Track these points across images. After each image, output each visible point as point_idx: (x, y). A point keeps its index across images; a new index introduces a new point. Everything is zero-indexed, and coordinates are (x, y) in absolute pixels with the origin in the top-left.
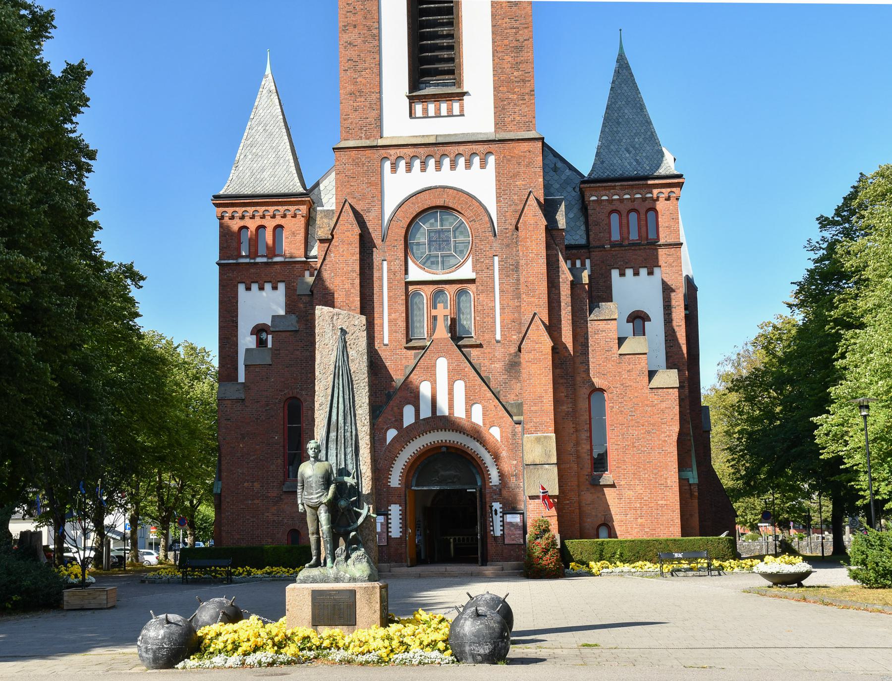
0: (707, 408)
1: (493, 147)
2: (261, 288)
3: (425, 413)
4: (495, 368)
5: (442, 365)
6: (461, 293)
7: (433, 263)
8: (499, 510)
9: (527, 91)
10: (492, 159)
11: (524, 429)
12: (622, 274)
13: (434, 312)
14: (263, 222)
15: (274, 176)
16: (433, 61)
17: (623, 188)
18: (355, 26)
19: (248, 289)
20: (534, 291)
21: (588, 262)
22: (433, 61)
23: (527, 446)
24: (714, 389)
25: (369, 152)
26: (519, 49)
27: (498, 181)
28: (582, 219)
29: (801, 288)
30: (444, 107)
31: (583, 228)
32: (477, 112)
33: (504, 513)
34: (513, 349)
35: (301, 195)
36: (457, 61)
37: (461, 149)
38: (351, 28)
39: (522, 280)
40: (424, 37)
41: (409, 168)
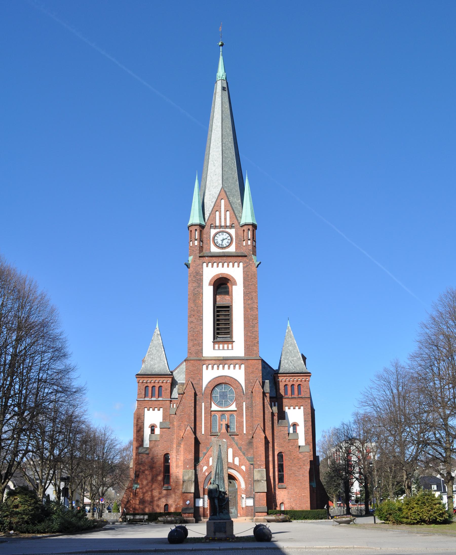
0: (318, 456)
1: (243, 362)
2: (154, 410)
7: (221, 404)
8: (244, 497)
9: (256, 342)
10: (243, 366)
11: (254, 467)
13: (221, 423)
15: (159, 367)
18: (194, 316)
21: (276, 403)
23: (255, 474)
24: (320, 440)
25: (198, 362)
27: (245, 374)
28: (274, 387)
30: (226, 346)
31: (275, 390)
32: (238, 348)
34: (250, 437)
35: (170, 375)
36: (230, 329)
37: (232, 362)
40: (218, 320)
41: (213, 368)
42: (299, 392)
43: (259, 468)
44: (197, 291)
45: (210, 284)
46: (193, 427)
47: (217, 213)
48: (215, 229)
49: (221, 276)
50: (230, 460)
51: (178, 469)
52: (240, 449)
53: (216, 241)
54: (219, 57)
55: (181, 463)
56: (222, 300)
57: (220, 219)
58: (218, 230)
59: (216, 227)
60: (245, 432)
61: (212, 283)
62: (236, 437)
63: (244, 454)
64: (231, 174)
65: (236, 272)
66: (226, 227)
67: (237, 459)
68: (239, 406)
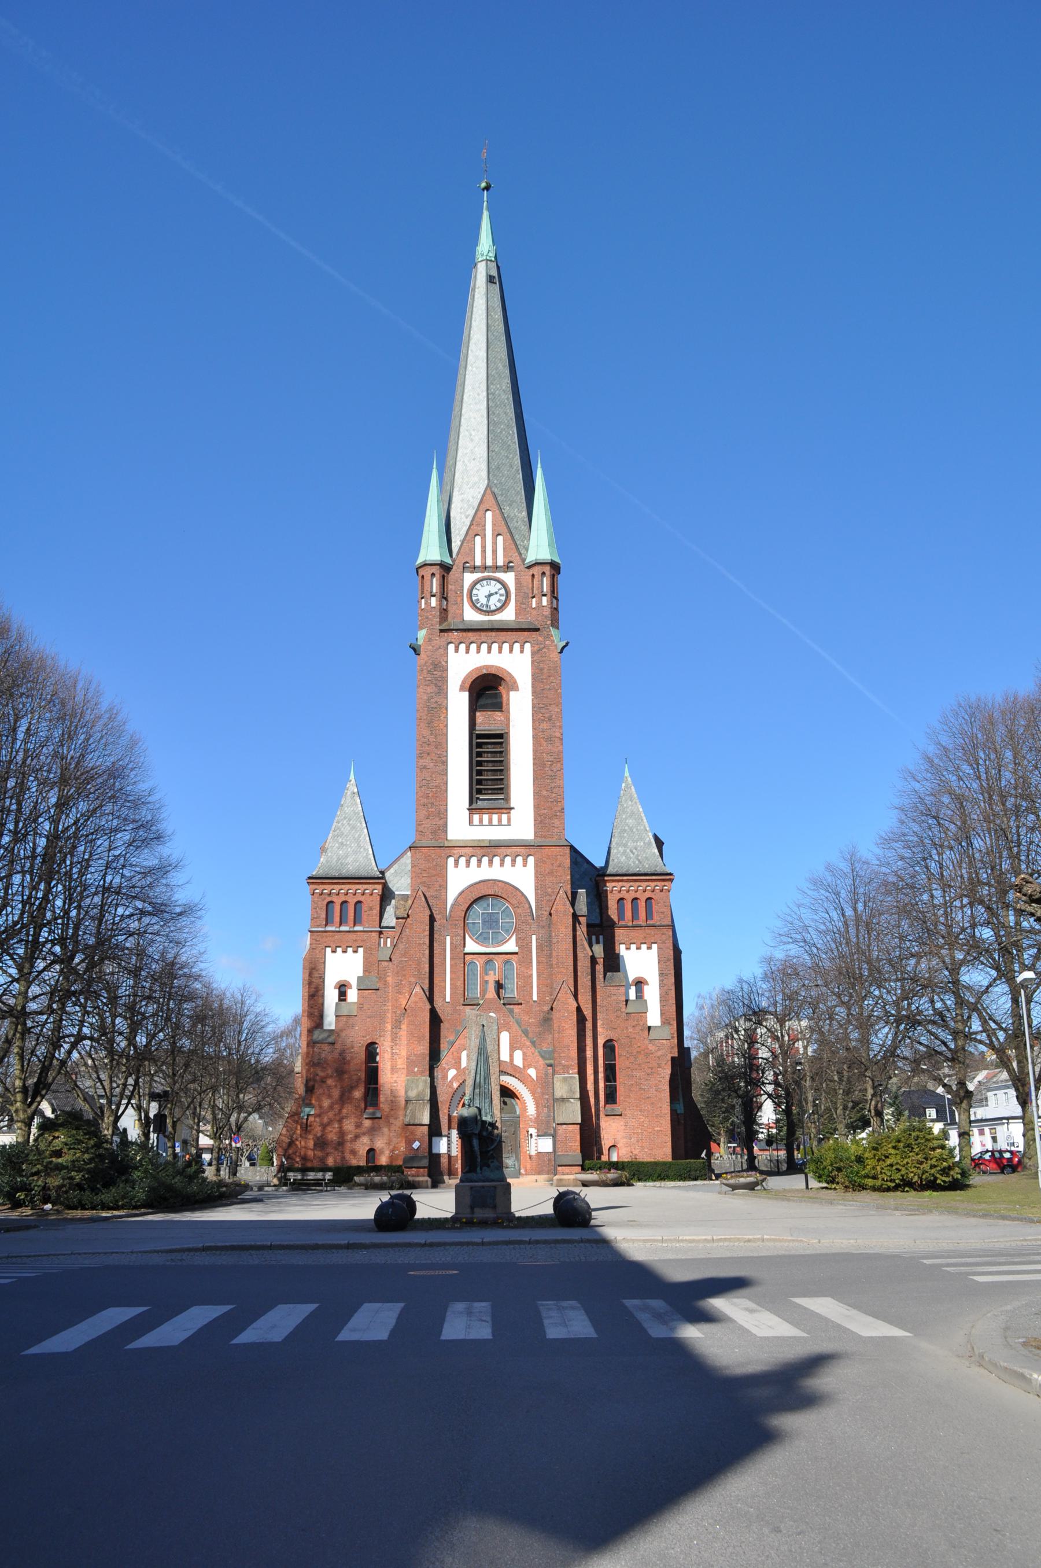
1: (532, 850)
2: (345, 952)
6: (507, 962)
7: (485, 938)
11: (554, 1071)
12: (457, 650)
13: (486, 978)
14: (347, 898)
16: (488, 780)
19: (334, 951)
21: (601, 937)
22: (488, 780)
23: (558, 1085)
25: (438, 850)
26: (553, 777)
28: (597, 903)
29: (500, 1142)
31: (598, 910)
32: (521, 822)
34: (547, 1008)
37: (509, 851)
38: (425, 755)
39: (554, 954)
42: (649, 914)
43: (564, 1073)
45: (462, 689)
46: (426, 987)
49: (484, 672)
52: (526, 1033)
53: (474, 598)
54: (482, 213)
55: (401, 1063)
56: (487, 721)
57: (484, 551)
59: (474, 569)
60: (535, 998)
61: (467, 686)
62: (516, 1009)
63: (533, 1043)
64: (507, 457)
65: (516, 662)
66: (496, 568)
67: (518, 1056)
68: (524, 944)
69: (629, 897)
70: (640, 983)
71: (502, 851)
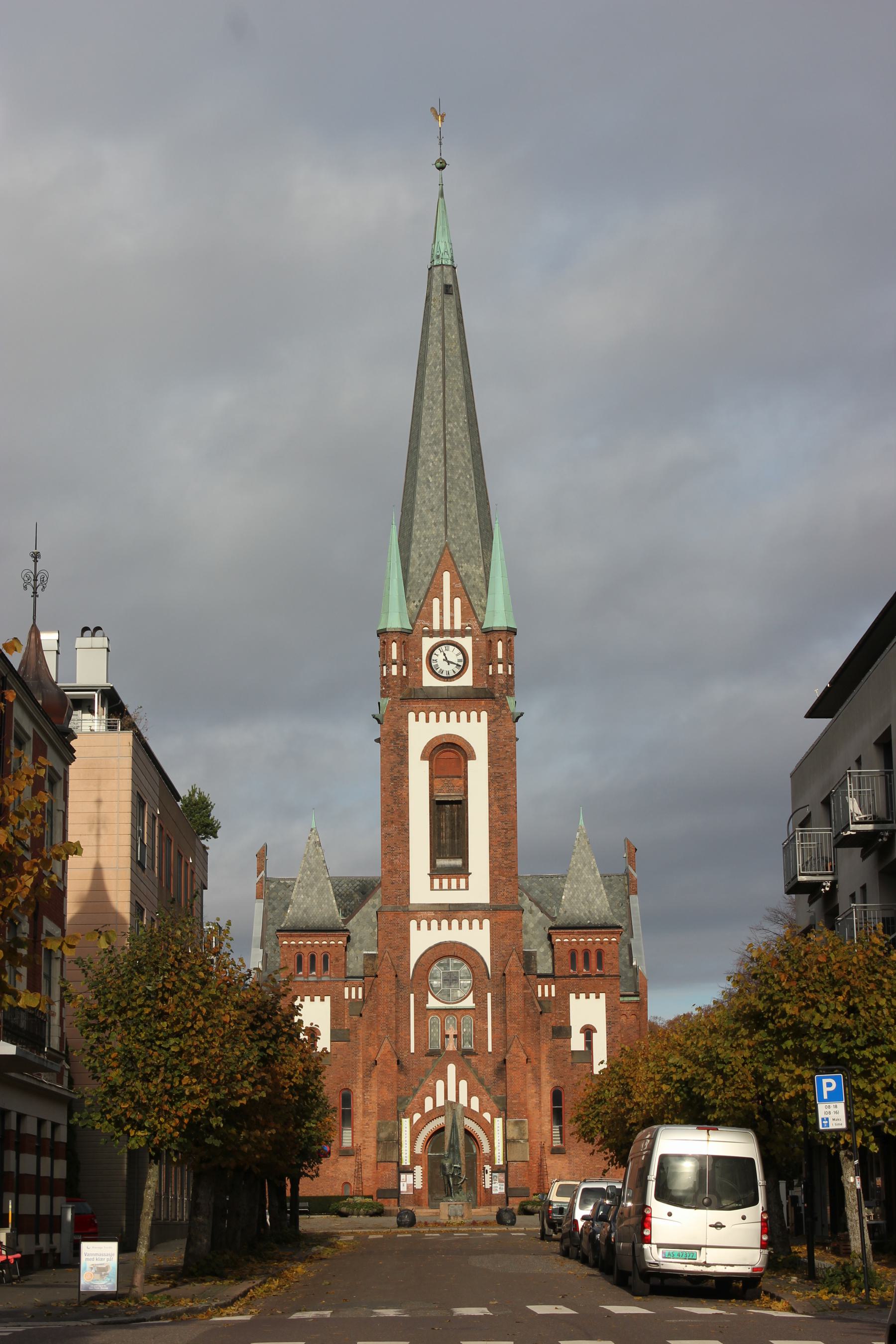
3: (440, 1102)
4: (488, 1071)
5: (451, 1069)
8: (489, 1171)
12: (578, 997)
17: (579, 934)
19: (578, 997)
20: (515, 1019)
31: (550, 960)
32: (478, 888)
33: (492, 1172)
42: (600, 964)
44: (399, 772)
45: (423, 758)
47: (436, 602)
48: (431, 637)
49: (444, 741)
50: (463, 1101)
51: (367, 1119)
52: (481, 1081)
53: (433, 664)
55: (373, 1108)
58: (437, 640)
59: (431, 634)
60: (490, 1050)
61: (427, 754)
62: (473, 1059)
63: (488, 1090)
64: (465, 506)
66: (453, 633)
67: (475, 1101)
68: (480, 1001)
69: (580, 949)
70: (588, 1031)
71: (461, 914)
